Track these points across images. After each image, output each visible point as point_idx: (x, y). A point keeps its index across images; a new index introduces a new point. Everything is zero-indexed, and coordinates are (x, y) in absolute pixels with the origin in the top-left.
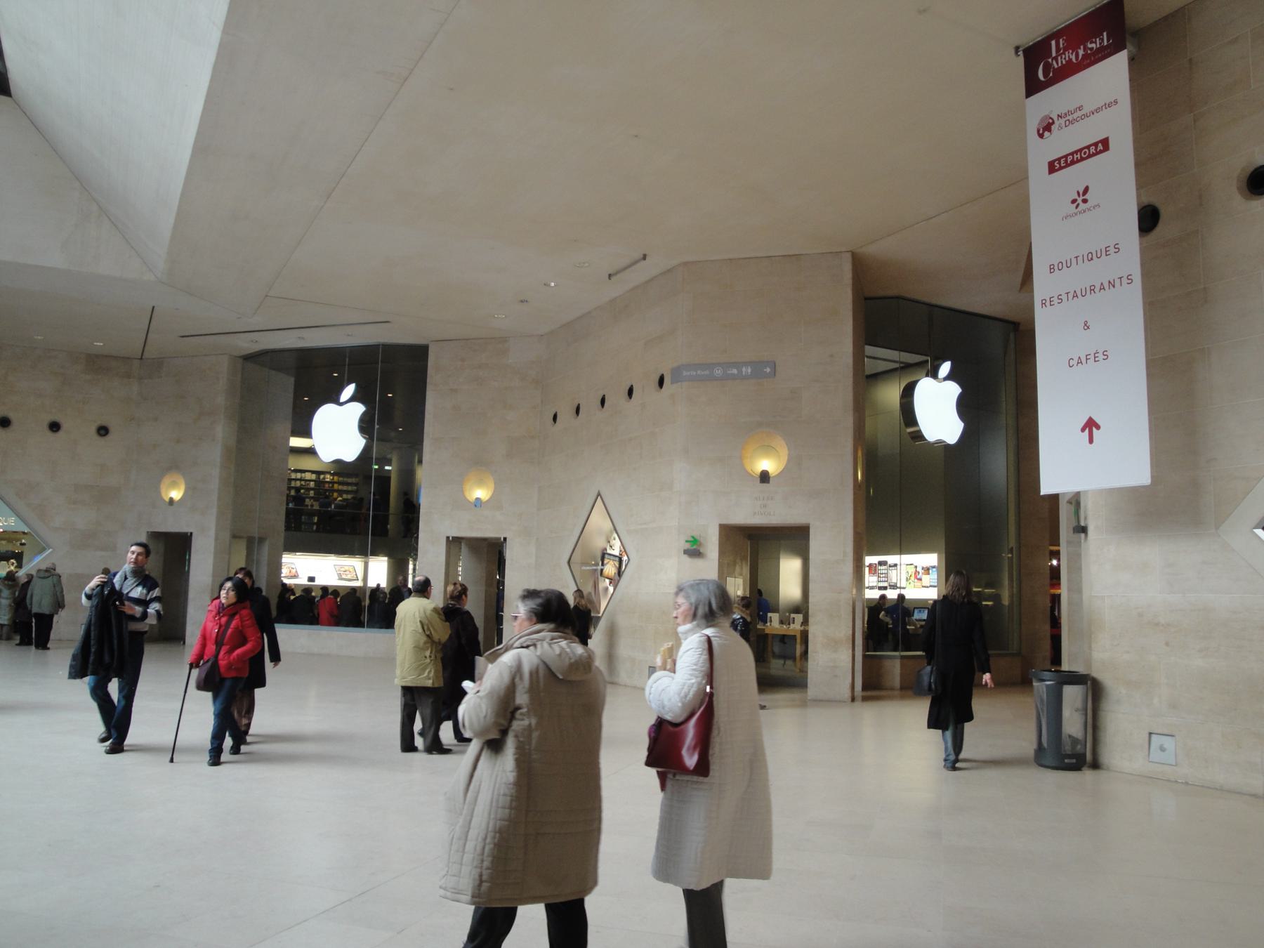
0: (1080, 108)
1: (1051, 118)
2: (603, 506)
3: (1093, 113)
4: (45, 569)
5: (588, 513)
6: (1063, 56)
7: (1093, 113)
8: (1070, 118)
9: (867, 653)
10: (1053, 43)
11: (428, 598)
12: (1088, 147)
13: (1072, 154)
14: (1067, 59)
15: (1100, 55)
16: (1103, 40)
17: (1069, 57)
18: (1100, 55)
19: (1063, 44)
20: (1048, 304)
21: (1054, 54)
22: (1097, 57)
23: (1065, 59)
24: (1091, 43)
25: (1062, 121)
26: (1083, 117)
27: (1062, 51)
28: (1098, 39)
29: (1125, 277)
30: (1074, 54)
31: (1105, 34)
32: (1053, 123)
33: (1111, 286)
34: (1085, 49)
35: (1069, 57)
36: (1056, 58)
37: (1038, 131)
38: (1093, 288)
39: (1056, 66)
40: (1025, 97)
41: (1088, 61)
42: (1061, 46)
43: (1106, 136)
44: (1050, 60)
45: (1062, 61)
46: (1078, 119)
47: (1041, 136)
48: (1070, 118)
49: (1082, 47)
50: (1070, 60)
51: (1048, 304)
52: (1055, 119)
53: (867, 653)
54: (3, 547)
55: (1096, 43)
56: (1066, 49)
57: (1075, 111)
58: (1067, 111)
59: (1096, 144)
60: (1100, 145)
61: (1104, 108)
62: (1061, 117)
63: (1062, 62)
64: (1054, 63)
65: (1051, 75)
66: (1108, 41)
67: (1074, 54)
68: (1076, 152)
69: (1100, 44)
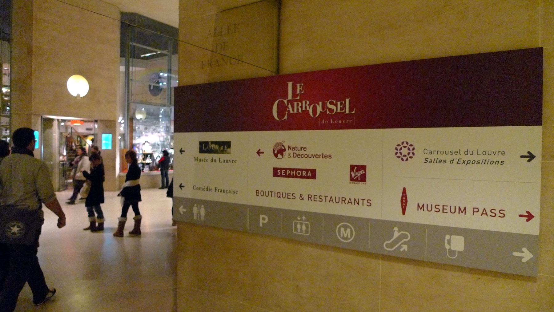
0: (305, 149)
1: (283, 146)
3: (313, 157)
4: (172, 69)
7: (313, 157)
8: (297, 152)
10: (290, 84)
12: (302, 170)
13: (290, 169)
14: (304, 109)
15: (340, 122)
16: (344, 106)
17: (306, 107)
18: (340, 122)
19: (301, 91)
20: (312, 198)
21: (290, 97)
22: (336, 122)
23: (301, 107)
24: (331, 103)
25: (291, 152)
26: (306, 156)
27: (298, 98)
28: (339, 103)
29: (366, 200)
30: (312, 106)
32: (285, 150)
33: (357, 200)
34: (323, 108)
35: (306, 107)
36: (292, 102)
37: (274, 151)
38: (344, 199)
40: (31, 157)
41: (327, 122)
42: (298, 92)
44: (286, 101)
45: (294, 109)
46: (302, 156)
47: (276, 156)
48: (297, 152)
50: (307, 112)
51: (312, 198)
52: (287, 148)
55: (336, 105)
57: (301, 149)
58: (295, 147)
59: (307, 171)
60: (309, 172)
61: (321, 156)
62: (291, 149)
63: (298, 109)
64: (290, 106)
65: (286, 118)
67: (312, 106)
68: (293, 170)
69: (341, 109)
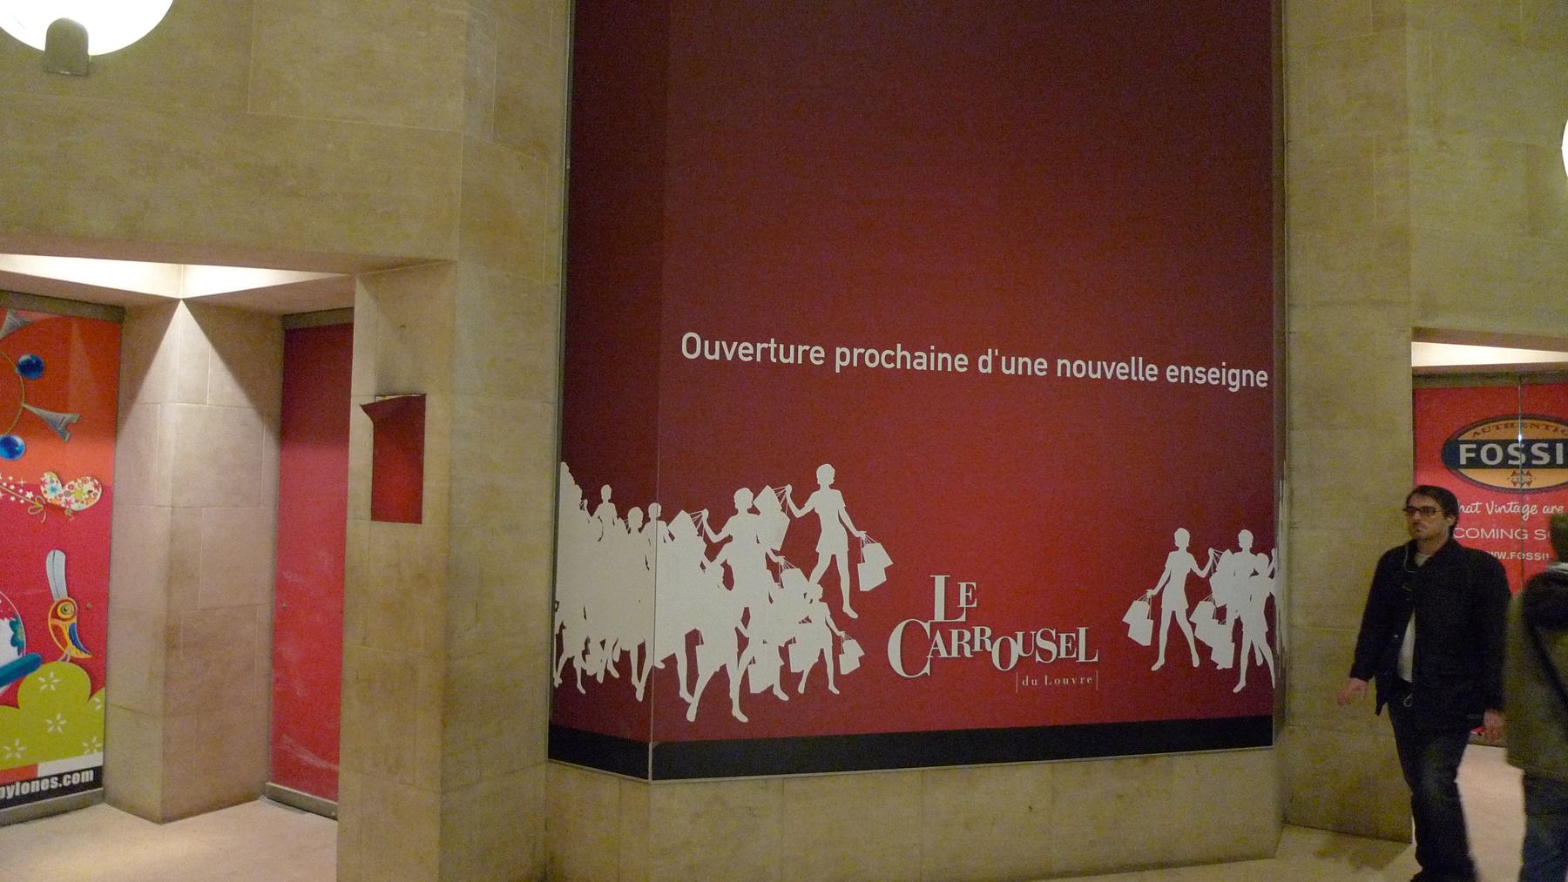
2: (559, 565)
5: (548, 538)
6: (967, 635)
9: (1235, 379)
11: (422, 399)
14: (977, 648)
19: (968, 601)
21: (939, 616)
23: (971, 643)
27: (963, 618)
28: (1063, 637)
31: (1082, 631)
36: (944, 629)
39: (944, 654)
43: (1223, 604)
44: (927, 626)
49: (1020, 635)
53: (1235, 379)
54: (1, 781)
55: (1057, 642)
56: (974, 619)
63: (961, 648)
65: (927, 670)
66: (1089, 655)
